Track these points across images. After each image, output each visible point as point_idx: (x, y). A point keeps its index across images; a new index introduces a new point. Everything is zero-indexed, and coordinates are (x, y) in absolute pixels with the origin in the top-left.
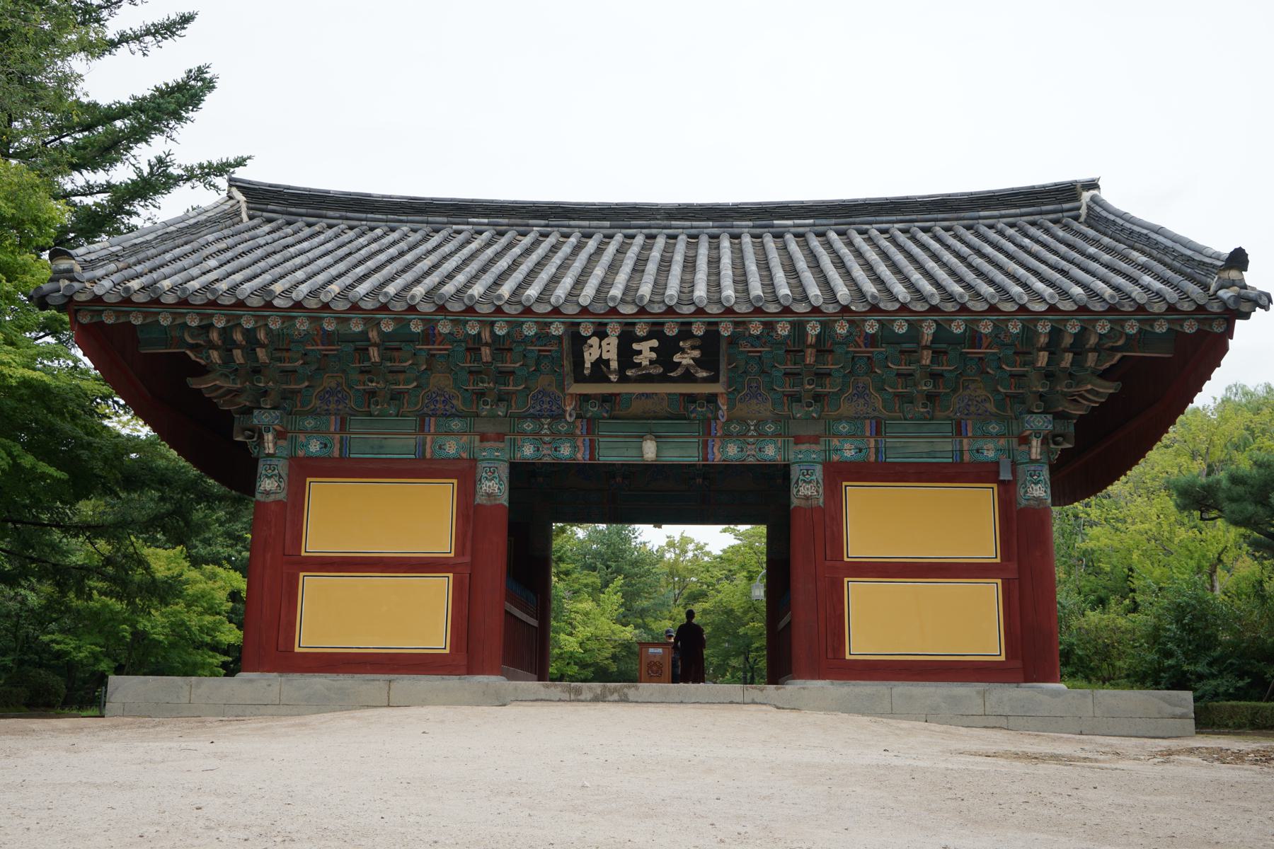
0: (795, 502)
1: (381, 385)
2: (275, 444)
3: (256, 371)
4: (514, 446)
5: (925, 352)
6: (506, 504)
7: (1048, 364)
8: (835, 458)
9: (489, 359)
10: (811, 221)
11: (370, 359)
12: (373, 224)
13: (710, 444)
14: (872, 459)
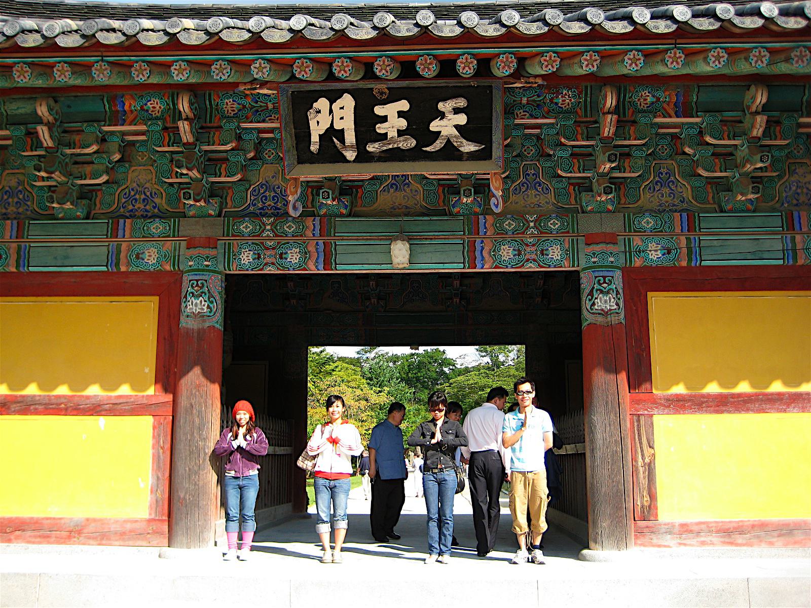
0: (588, 318)
4: (230, 255)
8: (637, 262)
13: (478, 246)
14: (684, 264)
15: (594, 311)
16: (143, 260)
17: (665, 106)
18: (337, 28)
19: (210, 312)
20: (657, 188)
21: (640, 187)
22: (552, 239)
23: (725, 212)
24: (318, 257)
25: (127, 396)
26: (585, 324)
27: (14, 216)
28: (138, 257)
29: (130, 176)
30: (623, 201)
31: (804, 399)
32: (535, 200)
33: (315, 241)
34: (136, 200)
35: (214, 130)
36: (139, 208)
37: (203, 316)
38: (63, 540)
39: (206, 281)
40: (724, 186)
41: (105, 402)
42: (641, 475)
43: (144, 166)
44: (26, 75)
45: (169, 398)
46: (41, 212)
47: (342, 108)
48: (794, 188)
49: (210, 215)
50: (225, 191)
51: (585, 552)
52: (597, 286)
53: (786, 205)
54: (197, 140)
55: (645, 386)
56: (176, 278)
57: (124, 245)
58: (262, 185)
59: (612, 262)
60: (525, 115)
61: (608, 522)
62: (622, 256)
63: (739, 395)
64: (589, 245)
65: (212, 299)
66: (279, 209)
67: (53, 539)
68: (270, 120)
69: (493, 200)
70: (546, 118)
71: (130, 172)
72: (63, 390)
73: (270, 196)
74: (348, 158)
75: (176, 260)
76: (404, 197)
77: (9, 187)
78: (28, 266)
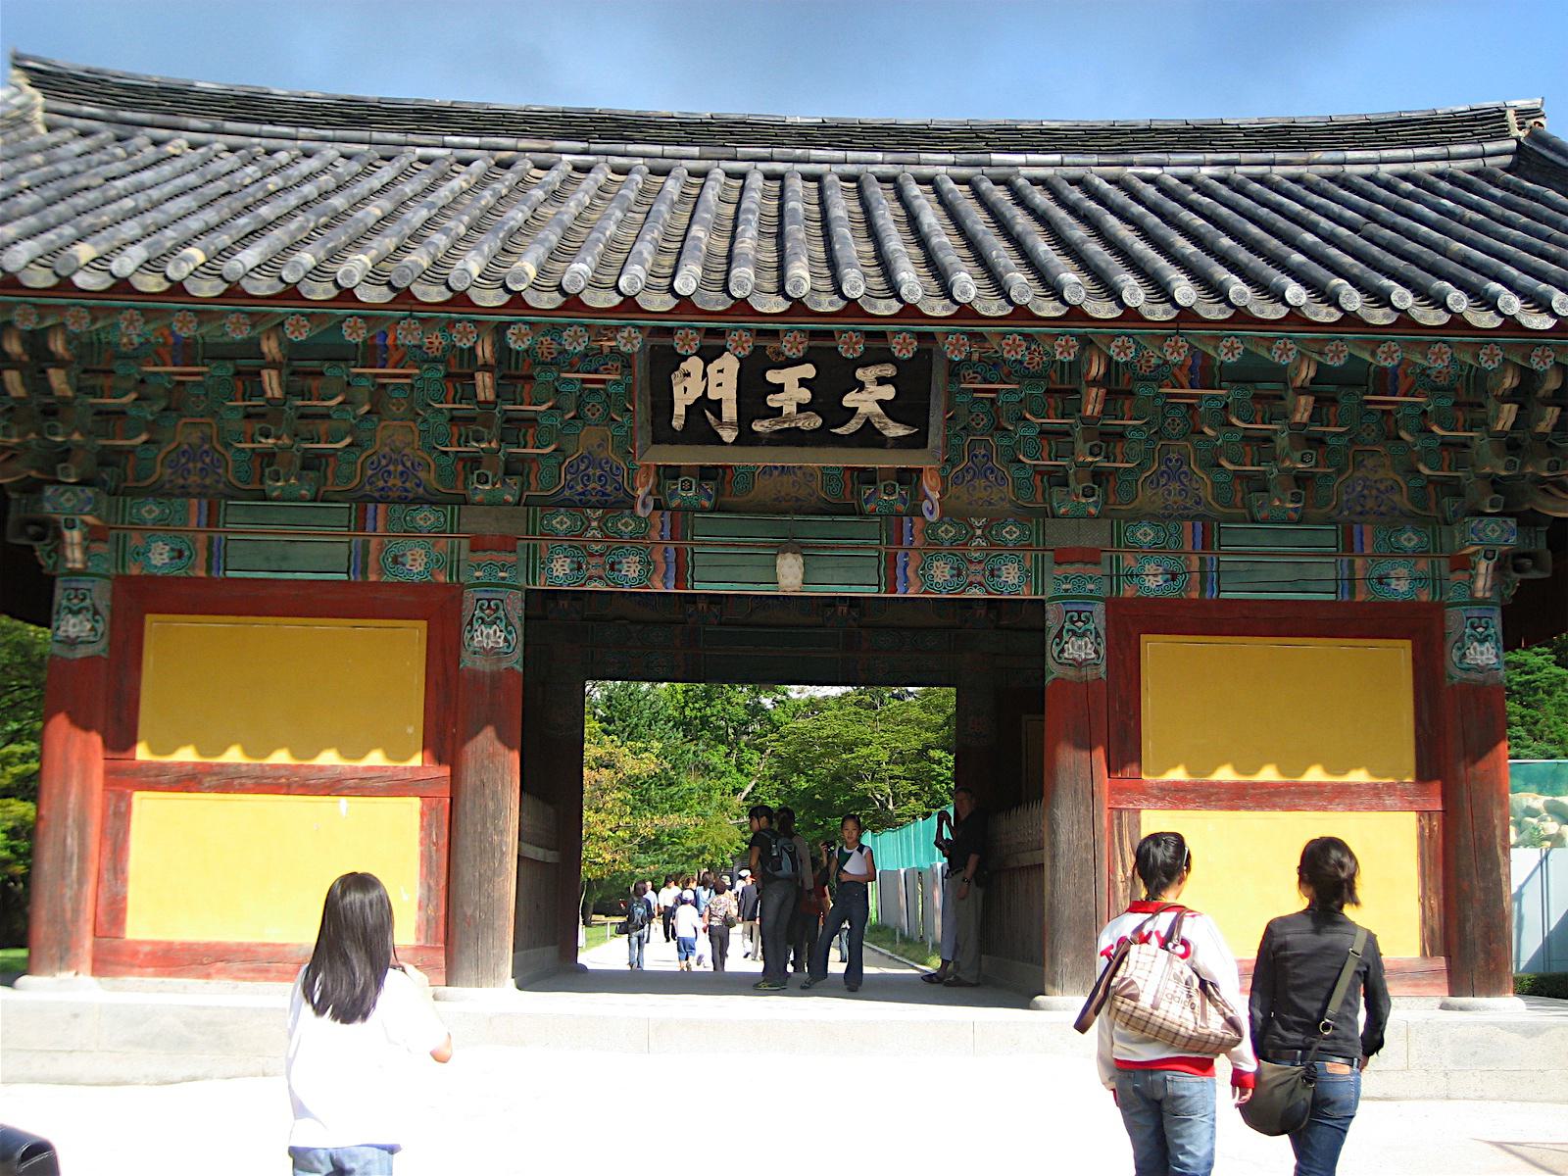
0: (1054, 670)
1: (286, 441)
2: (86, 550)
3: (49, 412)
4: (535, 563)
5: (1303, 400)
6: (519, 668)
7: (1514, 426)
8: (1127, 591)
9: (490, 396)
10: (1056, 158)
11: (263, 393)
12: (273, 143)
14: (1195, 595)
15: (1063, 661)
16: (404, 565)
17: (1176, 370)
18: (737, 296)
19: (508, 647)
20: (1163, 481)
21: (1137, 481)
22: (1006, 553)
23: (1257, 522)
24: (667, 569)
25: (381, 768)
26: (1049, 679)
27: (198, 490)
28: (395, 561)
29: (379, 435)
30: (1111, 501)
31: (1353, 793)
32: (984, 494)
33: (663, 546)
34: (389, 472)
35: (522, 381)
36: (394, 485)
37: (498, 653)
38: (287, 976)
39: (502, 601)
40: (1260, 484)
41: (349, 776)
42: (1121, 893)
43: (402, 420)
44: (303, 330)
45: (446, 771)
46: (240, 485)
47: (721, 371)
48: (1359, 489)
49: (506, 503)
50: (526, 465)
51: (1039, 998)
52: (1068, 625)
53: (1346, 513)
54: (498, 396)
55: (1129, 771)
56: (454, 593)
57: (374, 542)
58: (582, 458)
59: (1091, 591)
60: (975, 378)
61: (1072, 956)
62: (1106, 581)
63: (1264, 785)
64: (1059, 564)
65: (510, 628)
66: (609, 495)
67: (273, 975)
68: (606, 369)
69: (926, 504)
70: (1005, 383)
71: (379, 428)
72: (281, 757)
73: (594, 474)
74: (725, 439)
75: (454, 567)
76: (794, 482)
77: (190, 445)
78: (225, 570)
